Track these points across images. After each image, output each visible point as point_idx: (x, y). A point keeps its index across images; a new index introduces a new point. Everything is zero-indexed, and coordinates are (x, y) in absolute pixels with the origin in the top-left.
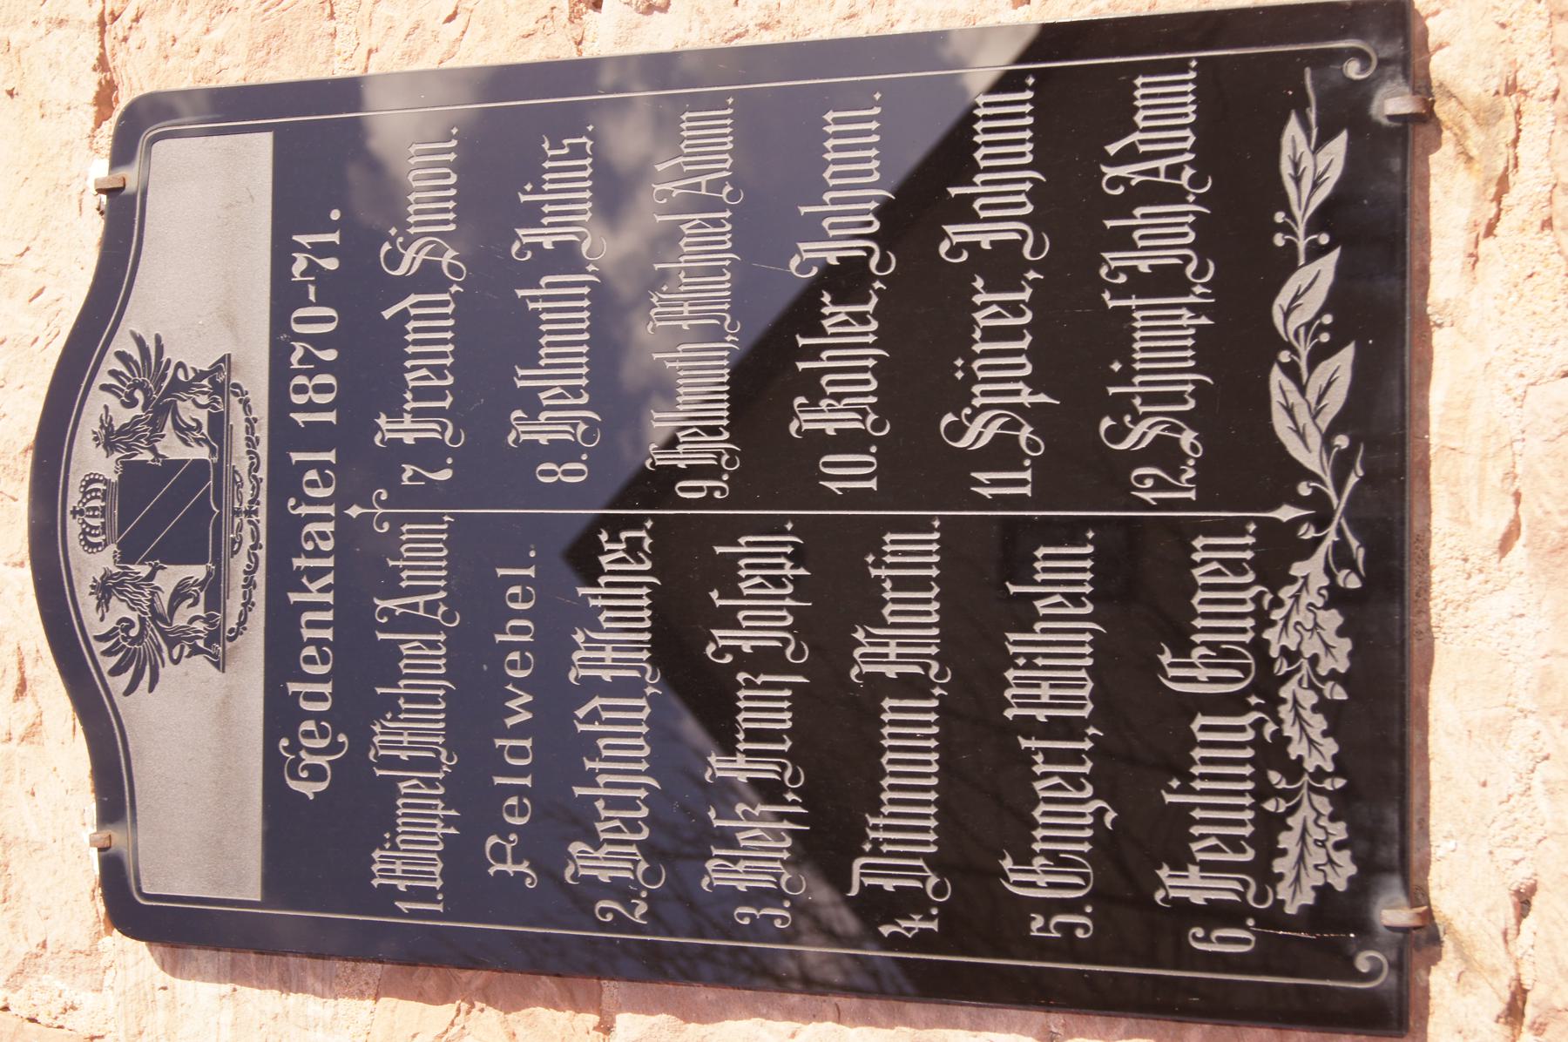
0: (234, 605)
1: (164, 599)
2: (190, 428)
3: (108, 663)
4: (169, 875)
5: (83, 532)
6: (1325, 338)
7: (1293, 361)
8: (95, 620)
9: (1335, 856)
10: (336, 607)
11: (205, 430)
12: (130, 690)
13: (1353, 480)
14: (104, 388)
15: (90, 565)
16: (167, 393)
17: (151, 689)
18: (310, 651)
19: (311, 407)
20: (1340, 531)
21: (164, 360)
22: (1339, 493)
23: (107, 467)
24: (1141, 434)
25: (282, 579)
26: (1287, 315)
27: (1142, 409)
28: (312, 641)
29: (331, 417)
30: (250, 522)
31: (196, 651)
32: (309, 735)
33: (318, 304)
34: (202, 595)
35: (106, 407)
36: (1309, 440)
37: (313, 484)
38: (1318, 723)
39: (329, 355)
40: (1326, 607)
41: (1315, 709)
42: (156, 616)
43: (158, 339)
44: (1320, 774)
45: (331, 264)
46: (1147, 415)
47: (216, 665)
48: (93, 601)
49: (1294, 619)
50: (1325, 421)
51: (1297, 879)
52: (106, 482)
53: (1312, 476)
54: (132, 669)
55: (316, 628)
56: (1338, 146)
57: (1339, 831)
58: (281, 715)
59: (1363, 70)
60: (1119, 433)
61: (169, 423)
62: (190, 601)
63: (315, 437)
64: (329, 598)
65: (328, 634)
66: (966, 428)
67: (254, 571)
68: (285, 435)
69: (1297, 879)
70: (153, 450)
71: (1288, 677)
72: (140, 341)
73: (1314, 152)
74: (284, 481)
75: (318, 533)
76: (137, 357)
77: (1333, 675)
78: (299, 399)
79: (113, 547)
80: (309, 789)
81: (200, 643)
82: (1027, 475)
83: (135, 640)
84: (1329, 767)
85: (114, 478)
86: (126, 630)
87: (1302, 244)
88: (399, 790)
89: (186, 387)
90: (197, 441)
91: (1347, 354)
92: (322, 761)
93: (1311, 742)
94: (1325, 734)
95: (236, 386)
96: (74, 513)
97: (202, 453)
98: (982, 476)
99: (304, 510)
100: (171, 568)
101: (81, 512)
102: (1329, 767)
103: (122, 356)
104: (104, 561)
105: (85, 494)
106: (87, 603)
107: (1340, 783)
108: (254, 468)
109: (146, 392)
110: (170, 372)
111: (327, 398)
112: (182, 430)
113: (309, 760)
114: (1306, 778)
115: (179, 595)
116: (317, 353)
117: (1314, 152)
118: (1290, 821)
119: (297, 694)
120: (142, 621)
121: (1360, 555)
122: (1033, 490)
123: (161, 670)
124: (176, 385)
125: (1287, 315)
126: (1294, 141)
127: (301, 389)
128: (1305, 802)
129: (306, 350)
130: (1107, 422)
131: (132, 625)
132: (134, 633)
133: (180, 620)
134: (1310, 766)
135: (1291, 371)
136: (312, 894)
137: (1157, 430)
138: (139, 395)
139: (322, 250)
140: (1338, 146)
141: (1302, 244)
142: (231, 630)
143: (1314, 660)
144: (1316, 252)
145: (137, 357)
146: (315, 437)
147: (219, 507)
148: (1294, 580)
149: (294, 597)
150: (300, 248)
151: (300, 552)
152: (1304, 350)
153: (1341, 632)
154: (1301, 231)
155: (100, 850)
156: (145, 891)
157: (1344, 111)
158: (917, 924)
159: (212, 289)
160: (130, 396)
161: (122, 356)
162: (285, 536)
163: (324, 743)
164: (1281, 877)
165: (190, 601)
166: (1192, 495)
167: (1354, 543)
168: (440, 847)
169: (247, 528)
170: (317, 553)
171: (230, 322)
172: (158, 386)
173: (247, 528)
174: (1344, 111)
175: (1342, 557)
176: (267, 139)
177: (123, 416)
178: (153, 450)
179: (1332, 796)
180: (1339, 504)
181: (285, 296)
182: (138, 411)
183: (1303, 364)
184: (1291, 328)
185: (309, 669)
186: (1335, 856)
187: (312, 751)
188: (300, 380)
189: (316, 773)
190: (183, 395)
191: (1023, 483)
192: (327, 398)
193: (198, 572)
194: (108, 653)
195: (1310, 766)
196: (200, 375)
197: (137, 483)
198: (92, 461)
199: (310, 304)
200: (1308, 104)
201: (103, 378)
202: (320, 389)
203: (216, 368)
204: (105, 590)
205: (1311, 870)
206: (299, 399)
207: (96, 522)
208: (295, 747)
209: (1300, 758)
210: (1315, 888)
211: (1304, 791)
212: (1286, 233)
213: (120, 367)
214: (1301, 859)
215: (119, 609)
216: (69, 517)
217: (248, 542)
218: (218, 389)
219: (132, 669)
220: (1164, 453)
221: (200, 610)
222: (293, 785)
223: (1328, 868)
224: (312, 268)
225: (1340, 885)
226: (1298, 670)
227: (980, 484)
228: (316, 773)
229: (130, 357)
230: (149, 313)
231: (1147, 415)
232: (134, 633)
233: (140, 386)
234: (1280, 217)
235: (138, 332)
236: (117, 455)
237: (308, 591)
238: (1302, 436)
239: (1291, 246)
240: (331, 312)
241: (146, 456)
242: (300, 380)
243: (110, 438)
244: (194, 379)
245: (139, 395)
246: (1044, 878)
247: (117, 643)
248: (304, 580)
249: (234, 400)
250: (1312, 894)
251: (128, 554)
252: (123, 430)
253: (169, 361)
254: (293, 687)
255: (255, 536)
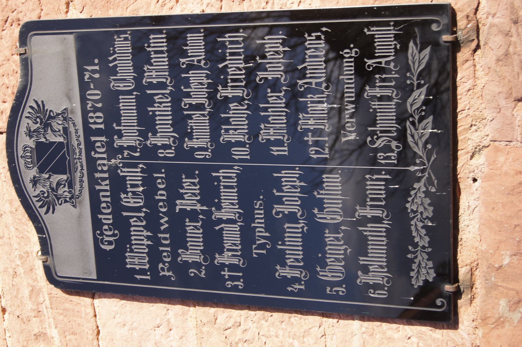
0: (77, 187)
1: (54, 185)
2: (56, 131)
3: (39, 204)
4: (66, 271)
5: (25, 163)
6: (423, 113)
7: (413, 120)
8: (32, 192)
9: (429, 271)
10: (111, 191)
11: (62, 132)
12: (47, 212)
13: (433, 159)
14: (26, 117)
15: (29, 174)
16: (48, 120)
17: (53, 213)
18: (104, 205)
19: (95, 123)
20: (429, 174)
21: (46, 108)
22: (428, 162)
23: (31, 143)
24: (379, 143)
25: (93, 182)
26: (412, 105)
27: (380, 135)
28: (104, 202)
29: (102, 126)
30: (80, 162)
31: (66, 201)
32: (106, 230)
33: (95, 89)
34: (67, 184)
35: (28, 123)
36: (419, 146)
37: (99, 147)
38: (423, 232)
39: (100, 105)
40: (425, 197)
41: (422, 227)
42: (52, 189)
43: (42, 102)
44: (424, 247)
45: (97, 76)
46: (381, 137)
47: (74, 206)
48: (31, 185)
49: (415, 201)
50: (424, 139)
51: (417, 277)
52: (31, 148)
53: (421, 157)
54: (46, 207)
55: (105, 198)
56: (427, 51)
57: (430, 264)
58: (97, 224)
59: (439, 27)
60: (373, 142)
61: (49, 129)
62: (63, 186)
63: (98, 132)
64: (108, 188)
65: (109, 199)
66: (376, 142)
67: (83, 177)
68: (88, 132)
69: (417, 277)
70: (45, 138)
71: (414, 217)
72: (36, 102)
73: (420, 52)
74: (90, 146)
75: (102, 164)
76: (36, 108)
77: (427, 218)
78: (91, 121)
79: (36, 168)
80: (109, 248)
81: (68, 199)
82: (286, 149)
83: (48, 197)
84: (427, 245)
85: (34, 147)
86: (43, 194)
87: (415, 83)
88: (130, 223)
89: (54, 118)
90: (60, 135)
91: (431, 118)
92: (111, 239)
93: (421, 236)
94: (425, 235)
95: (70, 118)
96: (22, 157)
97: (61, 140)
98: (274, 149)
99: (97, 156)
100: (56, 176)
101: (24, 157)
102: (427, 245)
103: (31, 107)
104: (33, 172)
105: (24, 151)
106: (29, 186)
107: (430, 250)
108: (79, 144)
109: (41, 119)
110: (48, 113)
111: (101, 121)
112: (53, 131)
113: (106, 239)
114: (419, 248)
115: (59, 184)
116: (95, 105)
117: (420, 52)
118: (415, 260)
119: (101, 218)
120: (48, 192)
121: (436, 182)
122: (288, 153)
123: (56, 207)
124: (50, 117)
125: (412, 105)
126: (412, 48)
127: (92, 118)
128: (419, 255)
129: (90, 75)
130: (369, 139)
131: (45, 193)
132: (46, 195)
133: (60, 192)
134: (421, 244)
135: (413, 123)
136: (112, 277)
137: (384, 143)
138: (38, 120)
139: (94, 72)
140: (427, 51)
141: (415, 83)
142: (77, 195)
143: (422, 213)
144: (419, 86)
145: (36, 108)
146: (98, 132)
147: (69, 157)
148: (415, 189)
149: (98, 187)
150: (87, 70)
151: (97, 171)
152: (417, 117)
153: (430, 205)
154: (415, 79)
155: (43, 262)
156: (58, 275)
157: (430, 41)
158: (297, 286)
159: (58, 85)
160: (35, 120)
161: (31, 107)
162: (92, 163)
163: (111, 233)
164: (413, 277)
165: (63, 186)
166: (395, 162)
167: (434, 178)
168: (146, 251)
169: (79, 164)
170: (102, 171)
171: (69, 98)
172: (45, 118)
173: (79, 164)
174: (430, 41)
175: (429, 181)
176: (71, 39)
177: (34, 127)
178: (45, 138)
179: (428, 253)
180: (428, 165)
181: (84, 87)
182: (38, 125)
183: (416, 121)
184: (413, 110)
185: (104, 211)
186: (429, 271)
187: (107, 236)
188: (91, 114)
189: (110, 243)
190: (53, 120)
191: (285, 151)
192: (101, 121)
193: (64, 177)
194: (37, 201)
195: (421, 244)
196: (58, 114)
197: (41, 149)
198: (25, 141)
199: (92, 89)
200: (416, 37)
201: (26, 114)
202: (98, 117)
203: (63, 113)
204: (35, 182)
205: (422, 275)
206: (91, 121)
207: (29, 160)
208: (102, 234)
209: (418, 242)
210: (423, 280)
211: (419, 252)
212: (410, 80)
213: (31, 111)
214: (418, 272)
215: (40, 188)
216: (20, 158)
217: (79, 168)
218: (65, 119)
219: (46, 207)
220: (387, 148)
221: (66, 189)
222: (103, 247)
223: (426, 275)
224: (91, 77)
225: (431, 280)
226: (417, 215)
227: (273, 151)
228: (110, 243)
229: (34, 108)
230: (37, 93)
231: (381, 137)
232: (46, 195)
233: (38, 117)
234: (408, 74)
235: (36, 99)
236: (33, 139)
237: (102, 185)
238: (417, 144)
239: (412, 84)
240: (98, 92)
241: (43, 140)
242: (91, 114)
243: (30, 134)
244: (56, 115)
245: (38, 120)
246: (333, 271)
247: (40, 198)
248: (100, 181)
249: (70, 122)
250: (422, 282)
251: (41, 170)
252: (34, 131)
253: (47, 109)
254: (100, 216)
255: (82, 166)
